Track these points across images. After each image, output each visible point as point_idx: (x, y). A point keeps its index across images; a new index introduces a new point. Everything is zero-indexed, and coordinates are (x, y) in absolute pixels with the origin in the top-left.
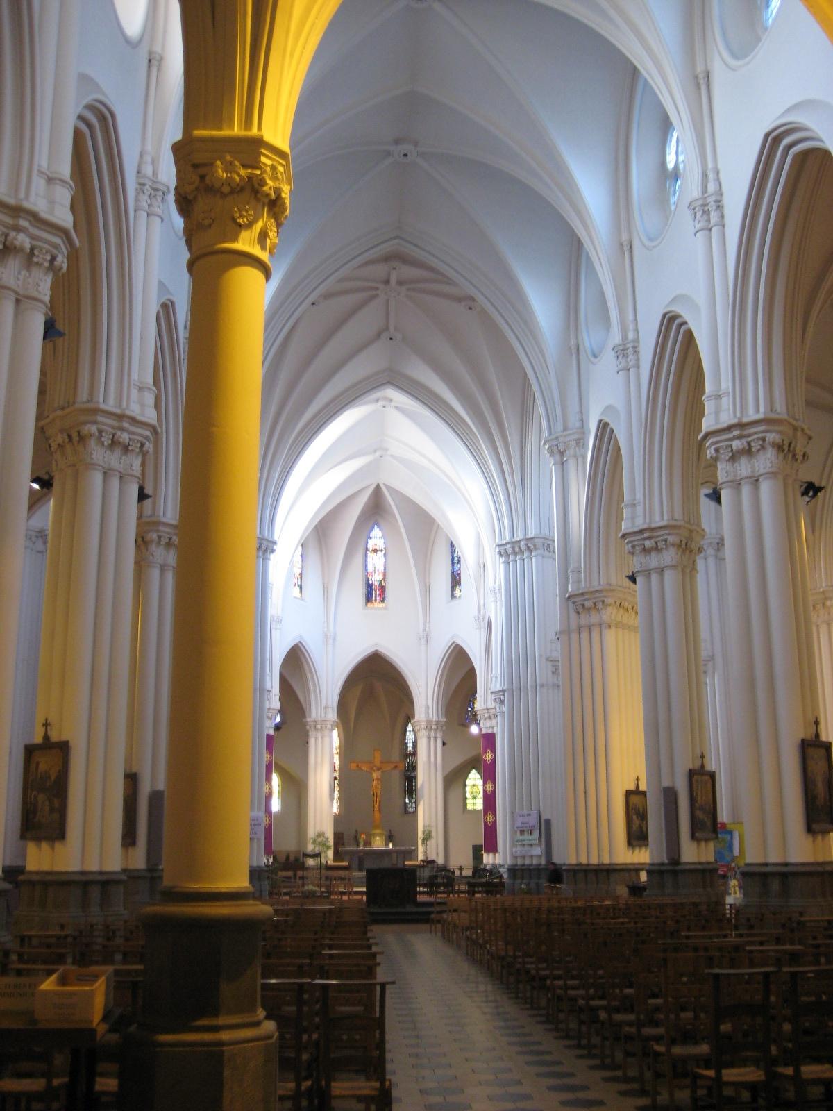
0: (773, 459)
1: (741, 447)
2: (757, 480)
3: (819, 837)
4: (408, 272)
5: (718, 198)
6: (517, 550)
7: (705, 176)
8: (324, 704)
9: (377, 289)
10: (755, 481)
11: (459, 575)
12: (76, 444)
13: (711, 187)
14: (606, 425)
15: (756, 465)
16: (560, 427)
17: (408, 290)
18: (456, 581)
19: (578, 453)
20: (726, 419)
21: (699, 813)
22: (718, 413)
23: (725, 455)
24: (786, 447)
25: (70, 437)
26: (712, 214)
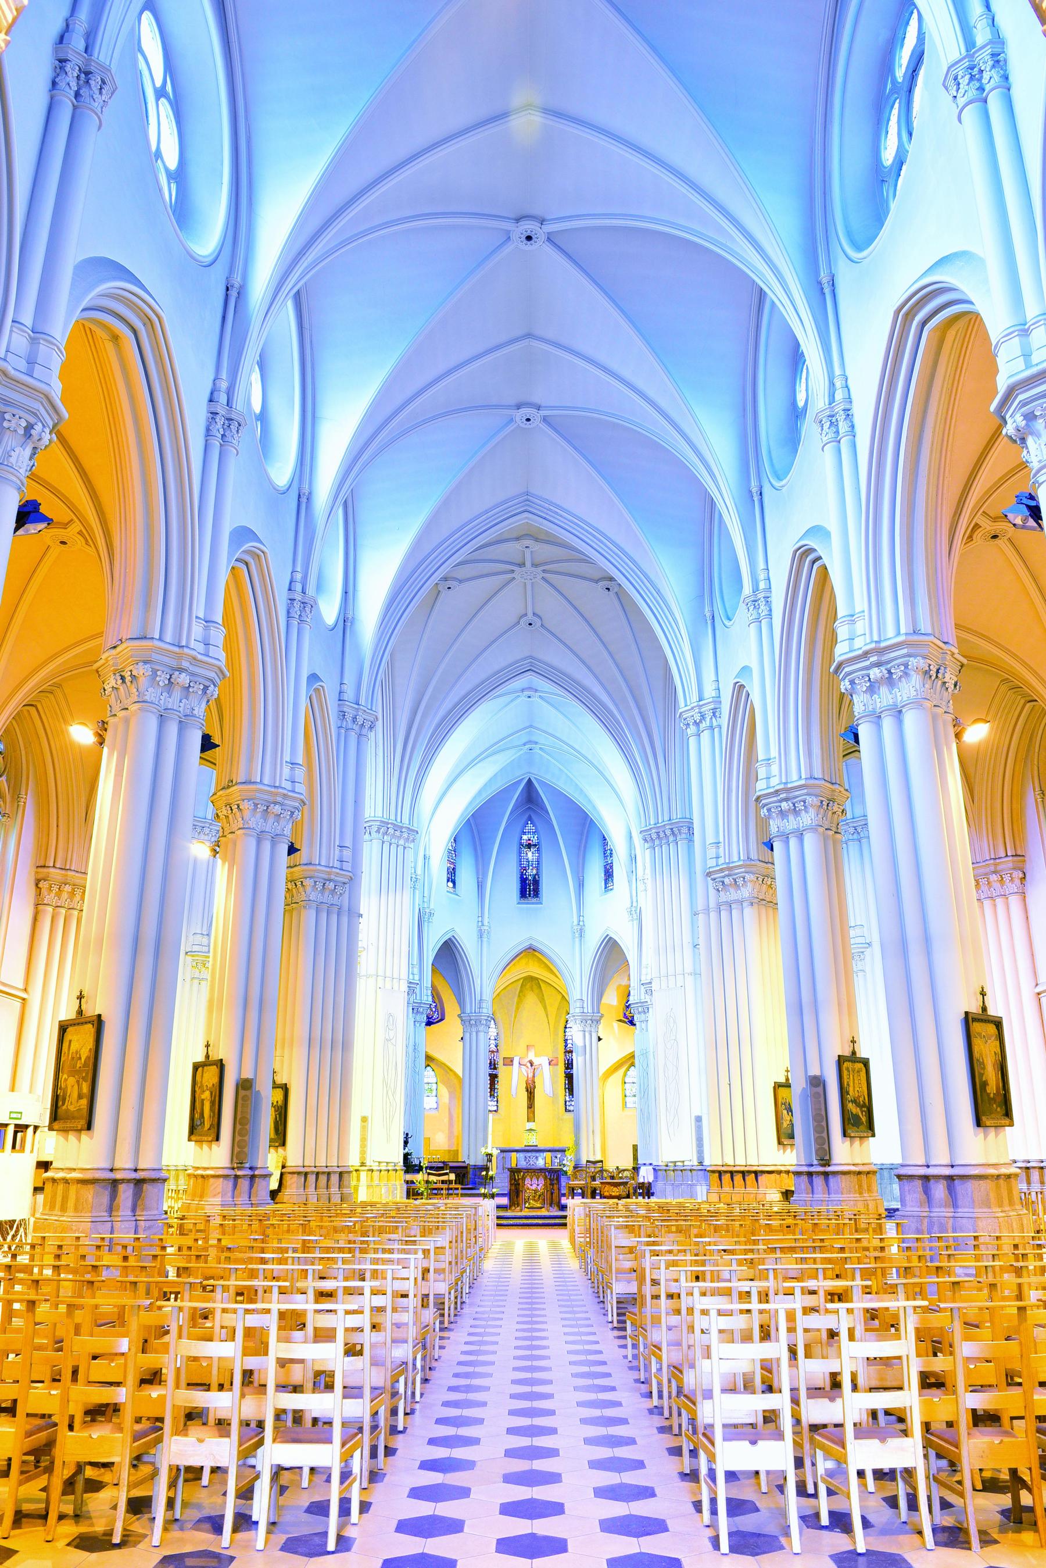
0: (918, 687)
1: (879, 675)
2: (900, 712)
3: (857, 1142)
4: (544, 551)
5: (848, 407)
6: (662, 835)
7: (832, 384)
8: (478, 998)
9: (513, 571)
10: (898, 713)
11: (611, 867)
12: (129, 684)
13: (839, 395)
14: (742, 686)
15: (899, 694)
16: (695, 697)
17: (544, 571)
18: (608, 874)
19: (715, 723)
20: (861, 644)
21: (851, 1106)
22: (852, 639)
23: (862, 686)
24: (933, 673)
25: (123, 678)
26: (841, 424)
